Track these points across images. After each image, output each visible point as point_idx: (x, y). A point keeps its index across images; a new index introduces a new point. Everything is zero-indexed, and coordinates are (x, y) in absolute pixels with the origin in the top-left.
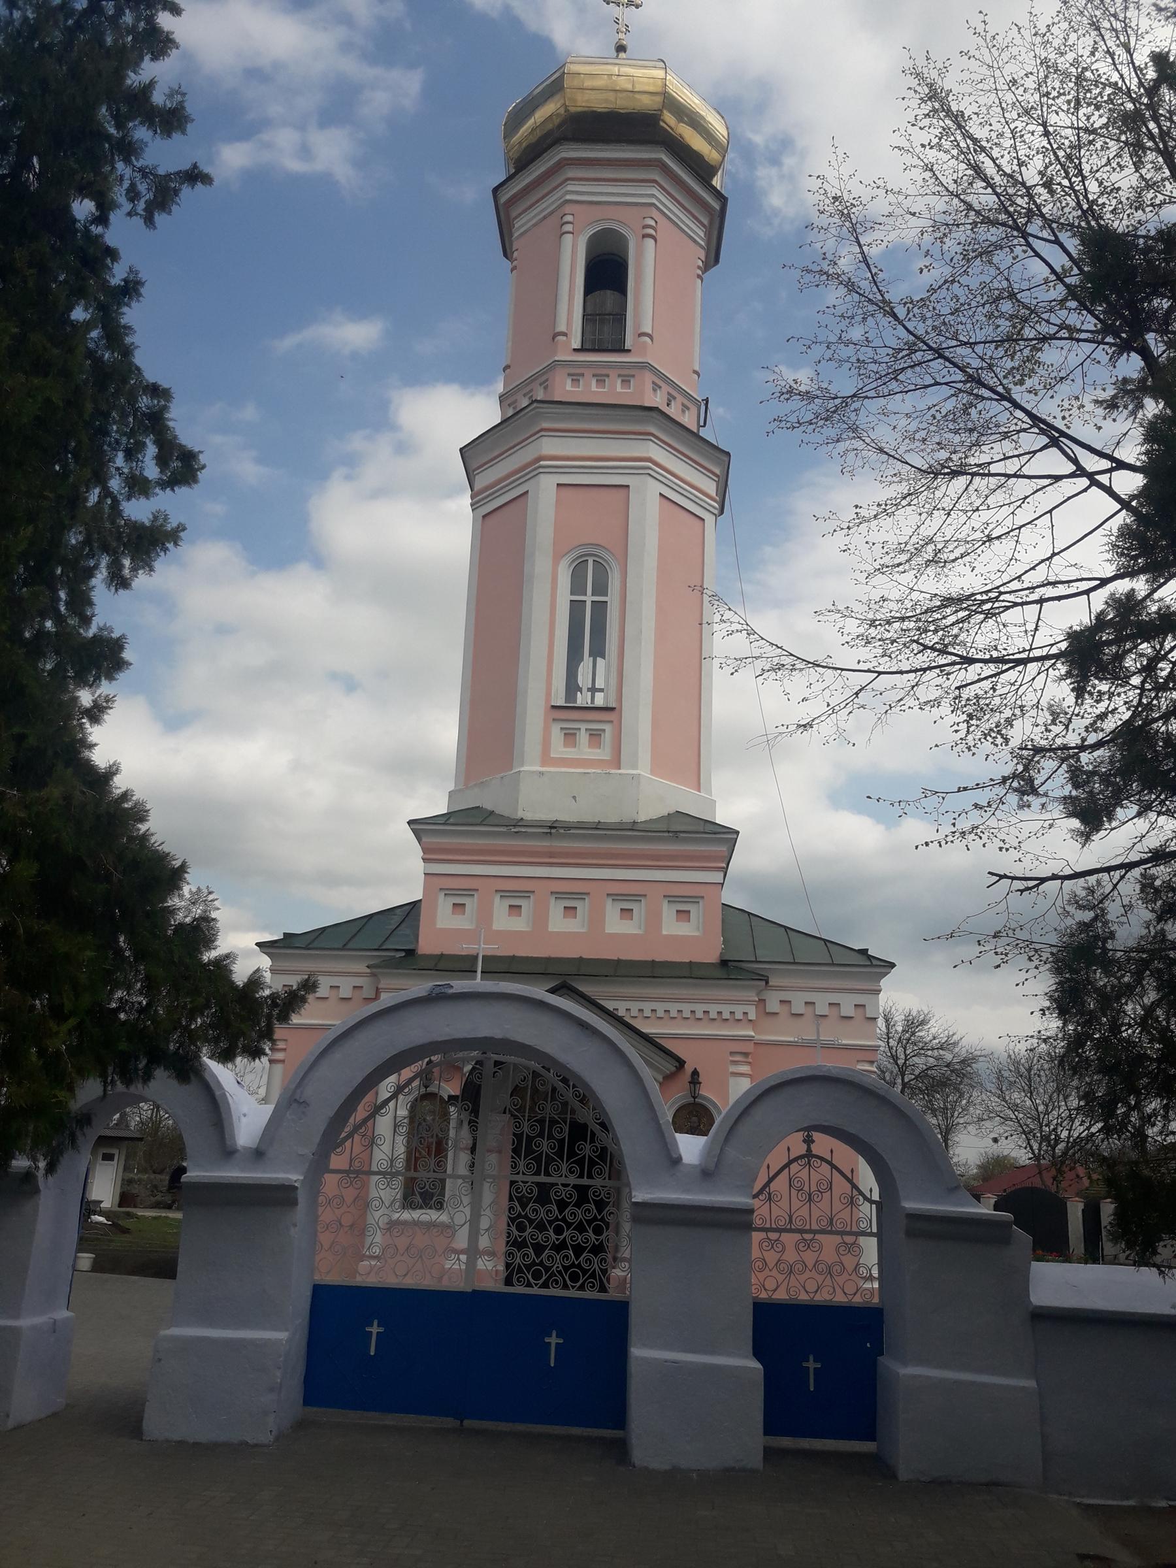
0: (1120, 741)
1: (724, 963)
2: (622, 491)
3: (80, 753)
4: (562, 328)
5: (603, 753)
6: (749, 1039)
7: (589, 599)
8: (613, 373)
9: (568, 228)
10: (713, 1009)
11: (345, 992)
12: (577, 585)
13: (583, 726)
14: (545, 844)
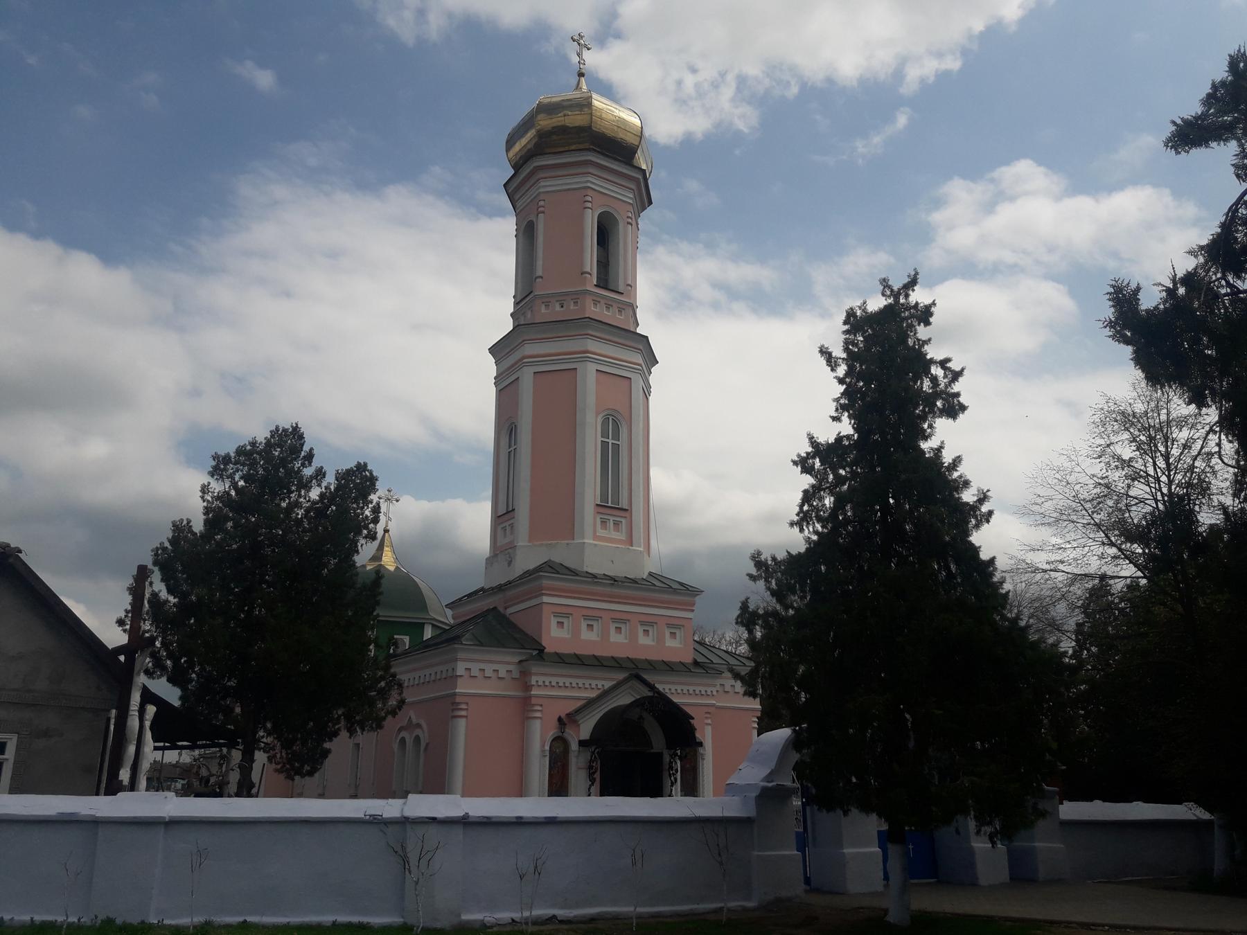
0: (233, 493)
1: (696, 663)
2: (627, 382)
3: (969, 535)
4: (588, 270)
5: (622, 536)
6: (713, 705)
7: (611, 441)
8: (615, 305)
9: (589, 205)
10: (698, 689)
11: (502, 674)
12: (605, 434)
13: (612, 519)
14: (608, 590)
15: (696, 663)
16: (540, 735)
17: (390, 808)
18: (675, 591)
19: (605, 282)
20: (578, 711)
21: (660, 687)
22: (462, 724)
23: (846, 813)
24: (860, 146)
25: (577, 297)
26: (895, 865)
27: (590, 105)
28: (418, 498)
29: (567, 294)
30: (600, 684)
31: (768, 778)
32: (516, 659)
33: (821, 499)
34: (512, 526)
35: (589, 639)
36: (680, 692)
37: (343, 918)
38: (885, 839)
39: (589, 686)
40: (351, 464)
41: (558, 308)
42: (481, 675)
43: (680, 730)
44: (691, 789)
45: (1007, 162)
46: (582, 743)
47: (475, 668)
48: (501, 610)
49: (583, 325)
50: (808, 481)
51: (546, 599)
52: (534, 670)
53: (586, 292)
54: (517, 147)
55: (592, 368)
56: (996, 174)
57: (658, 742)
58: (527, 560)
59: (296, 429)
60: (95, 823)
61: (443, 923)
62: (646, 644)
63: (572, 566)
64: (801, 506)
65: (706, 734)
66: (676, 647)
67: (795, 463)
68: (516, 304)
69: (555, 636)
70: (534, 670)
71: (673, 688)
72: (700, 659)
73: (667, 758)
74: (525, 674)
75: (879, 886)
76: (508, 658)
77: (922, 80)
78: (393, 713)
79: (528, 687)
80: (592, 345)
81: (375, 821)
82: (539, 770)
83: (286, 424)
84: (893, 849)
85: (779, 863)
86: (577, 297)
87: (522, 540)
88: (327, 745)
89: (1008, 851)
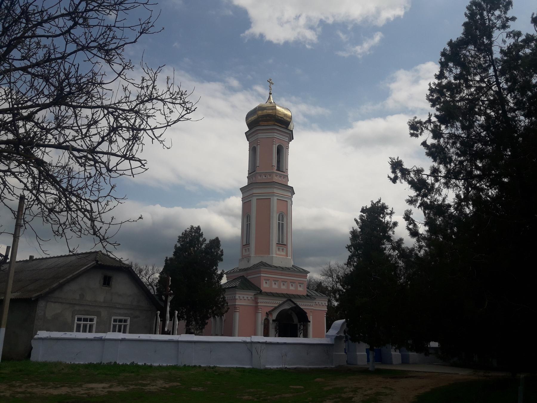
1: (307, 295)
5: (284, 253)
12: (279, 220)
15: (307, 295)
16: (261, 318)
17: (248, 339)
18: (301, 272)
19: (278, 169)
20: (273, 310)
21: (298, 303)
22: (237, 314)
23: (359, 343)
24: (358, 49)
25: (271, 174)
26: (371, 357)
27: (275, 109)
28: (162, 205)
29: (266, 173)
30: (279, 302)
31: (338, 333)
32: (253, 294)
33: (354, 259)
34: (249, 249)
35: (275, 288)
36: (303, 305)
37: (238, 366)
38: (367, 351)
39: (276, 302)
40: (214, 238)
41: (264, 177)
42: (243, 299)
43: (303, 317)
44: (306, 336)
45: (424, 62)
46: (273, 321)
47: (241, 296)
48: (245, 277)
49: (272, 184)
50: (350, 254)
51: (262, 275)
52: (259, 297)
53: (273, 172)
54: (250, 119)
55: (276, 198)
56: (418, 67)
57: (296, 320)
58: (255, 260)
59: (199, 227)
60: (178, 342)
61: (262, 368)
62: (292, 289)
63: (269, 263)
64: (348, 260)
65: (310, 318)
66: (302, 290)
67: (347, 248)
68: (249, 174)
69: (265, 286)
70: (259, 297)
71: (301, 303)
72: (309, 294)
73: (299, 326)
74: (256, 299)
75: (366, 363)
76: (251, 294)
77: (388, 19)
78: (226, 312)
79: (257, 303)
80: (275, 191)
81: (245, 343)
82: (260, 328)
83: (195, 225)
84: (371, 352)
85: (340, 356)
86: (271, 174)
87: (253, 255)
88: (207, 321)
89: (402, 355)
